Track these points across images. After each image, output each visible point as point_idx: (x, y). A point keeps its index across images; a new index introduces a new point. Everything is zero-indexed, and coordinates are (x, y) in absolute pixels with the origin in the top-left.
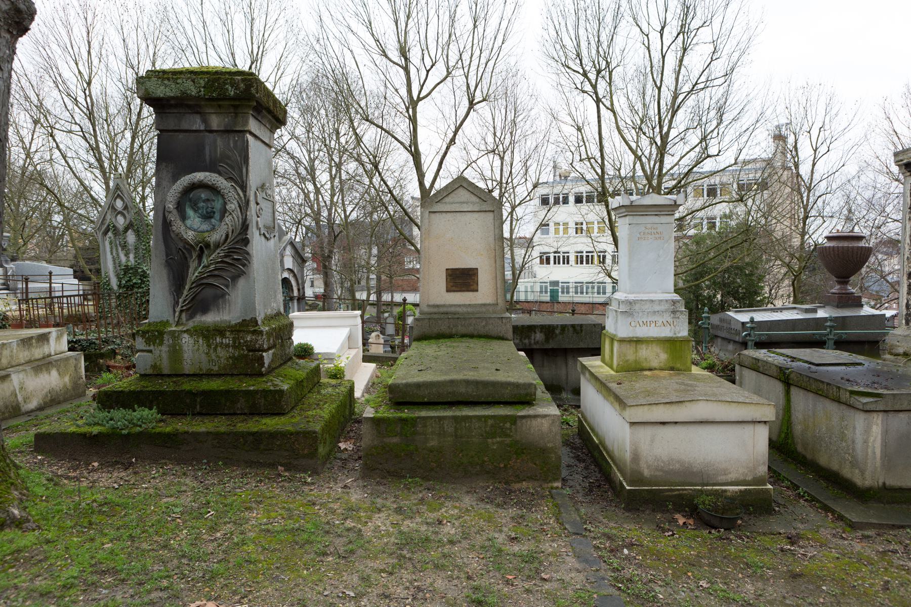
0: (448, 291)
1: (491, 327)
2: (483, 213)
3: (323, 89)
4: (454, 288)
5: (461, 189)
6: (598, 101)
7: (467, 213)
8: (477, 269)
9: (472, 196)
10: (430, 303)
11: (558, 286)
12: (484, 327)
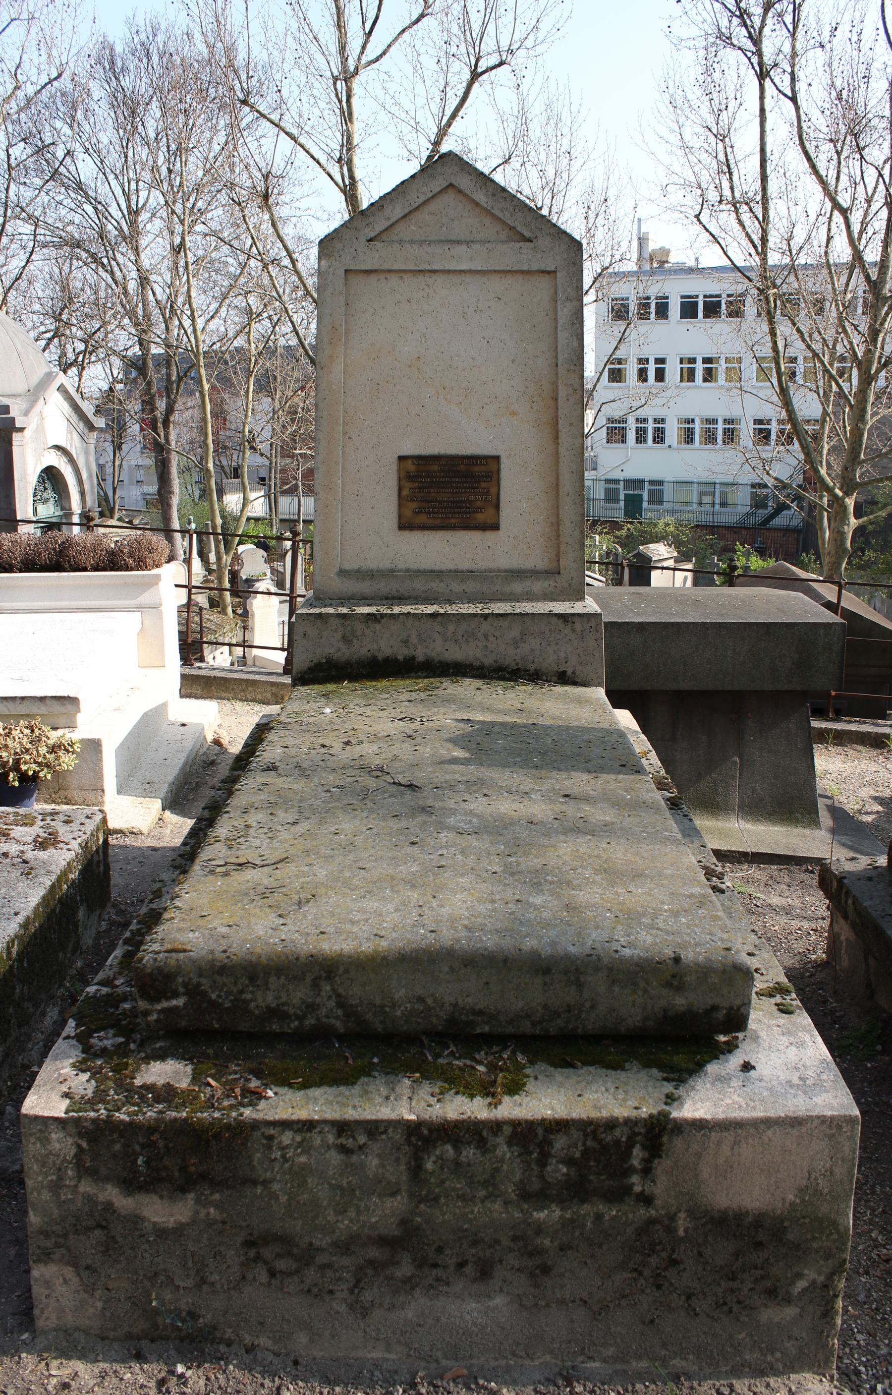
0: (404, 525)
1: (534, 643)
2: (520, 278)
4: (422, 519)
5: (450, 198)
6: (763, 75)
7: (468, 278)
8: (497, 458)
9: (487, 221)
10: (347, 566)
11: (643, 488)
12: (516, 643)
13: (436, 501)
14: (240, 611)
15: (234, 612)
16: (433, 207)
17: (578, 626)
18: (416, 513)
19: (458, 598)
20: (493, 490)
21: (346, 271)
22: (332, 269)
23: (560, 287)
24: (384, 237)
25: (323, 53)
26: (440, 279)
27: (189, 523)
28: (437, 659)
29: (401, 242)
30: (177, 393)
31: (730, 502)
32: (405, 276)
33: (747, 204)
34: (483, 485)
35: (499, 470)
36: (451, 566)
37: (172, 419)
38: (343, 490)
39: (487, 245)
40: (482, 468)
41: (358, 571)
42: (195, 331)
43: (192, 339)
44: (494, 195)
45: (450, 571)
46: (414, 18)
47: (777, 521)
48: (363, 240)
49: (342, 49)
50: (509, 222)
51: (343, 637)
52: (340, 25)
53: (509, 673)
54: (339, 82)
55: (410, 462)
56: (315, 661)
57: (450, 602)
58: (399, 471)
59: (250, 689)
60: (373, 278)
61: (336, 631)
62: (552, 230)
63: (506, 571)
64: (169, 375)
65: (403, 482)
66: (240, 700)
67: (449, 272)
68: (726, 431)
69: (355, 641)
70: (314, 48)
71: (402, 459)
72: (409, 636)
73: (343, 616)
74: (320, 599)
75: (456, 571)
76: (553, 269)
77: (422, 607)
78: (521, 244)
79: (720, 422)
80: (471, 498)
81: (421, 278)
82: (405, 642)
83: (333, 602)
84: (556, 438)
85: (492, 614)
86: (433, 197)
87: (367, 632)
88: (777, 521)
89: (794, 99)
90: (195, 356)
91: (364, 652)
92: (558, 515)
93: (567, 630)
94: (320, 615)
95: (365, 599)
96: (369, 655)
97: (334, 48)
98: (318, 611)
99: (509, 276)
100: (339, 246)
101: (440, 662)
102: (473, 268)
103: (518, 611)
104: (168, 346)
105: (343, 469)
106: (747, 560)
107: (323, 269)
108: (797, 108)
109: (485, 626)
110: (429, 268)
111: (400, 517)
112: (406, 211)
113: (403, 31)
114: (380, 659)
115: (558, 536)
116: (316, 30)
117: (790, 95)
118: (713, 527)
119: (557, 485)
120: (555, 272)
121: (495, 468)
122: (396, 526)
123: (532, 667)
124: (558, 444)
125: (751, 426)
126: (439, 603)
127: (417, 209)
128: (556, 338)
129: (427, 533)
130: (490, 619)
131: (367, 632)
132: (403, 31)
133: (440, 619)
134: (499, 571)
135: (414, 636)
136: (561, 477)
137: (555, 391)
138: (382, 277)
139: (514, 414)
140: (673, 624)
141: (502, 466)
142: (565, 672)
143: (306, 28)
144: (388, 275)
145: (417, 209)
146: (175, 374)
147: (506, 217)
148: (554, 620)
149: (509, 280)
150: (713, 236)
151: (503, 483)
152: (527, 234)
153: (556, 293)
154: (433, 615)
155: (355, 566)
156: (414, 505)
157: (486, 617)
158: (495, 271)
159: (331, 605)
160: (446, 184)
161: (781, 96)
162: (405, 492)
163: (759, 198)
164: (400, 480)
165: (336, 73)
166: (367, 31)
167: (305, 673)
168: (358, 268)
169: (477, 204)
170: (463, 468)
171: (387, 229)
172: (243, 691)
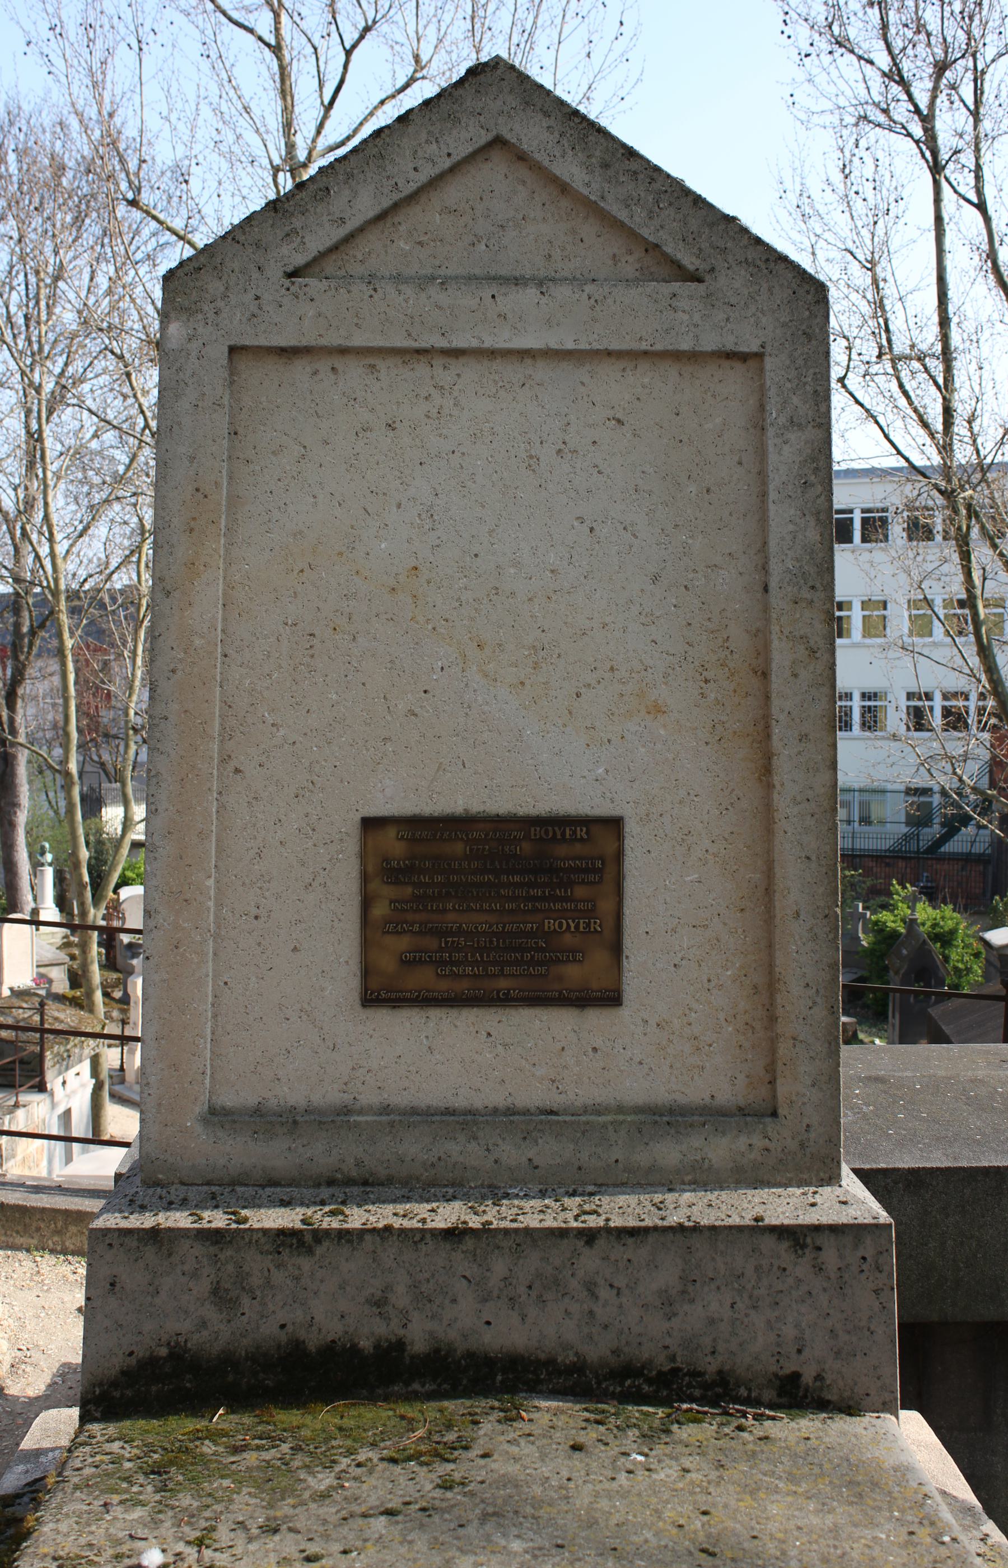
2: (671, 370)
3: (222, 553)
4: (424, 978)
7: (541, 371)
8: (615, 824)
9: (589, 229)
10: (228, 1099)
13: (460, 932)
14: (118, 994)
15: (106, 995)
16: (453, 193)
17: (830, 1257)
18: (408, 962)
19: (515, 1182)
20: (606, 906)
21: (232, 350)
22: (195, 345)
23: (772, 392)
24: (329, 266)
25: (257, 131)
26: (470, 372)
27: (43, 853)
28: (461, 1347)
29: (371, 279)
30: (29, 653)
31: (874, 817)
32: (381, 364)
33: (919, 359)
34: (580, 892)
35: (619, 856)
36: (497, 1098)
37: (20, 691)
38: (219, 905)
39: (589, 288)
40: (578, 848)
41: (258, 1112)
42: (52, 554)
43: (47, 563)
44: (606, 166)
45: (495, 1111)
46: (399, 84)
47: (955, 846)
48: (275, 272)
49: (288, 126)
50: (645, 232)
51: (216, 1291)
52: (285, 92)
53: (649, 1381)
54: (281, 175)
55: (392, 832)
56: (141, 1353)
57: (497, 1194)
58: (363, 856)
59: (73, 1229)
60: (300, 369)
61: (195, 1275)
62: (752, 254)
63: (638, 1110)
64: (17, 626)
65: (374, 885)
66: (52, 1251)
67: (493, 353)
68: (866, 711)
69: (246, 1301)
70: (243, 123)
71: (370, 824)
72: (388, 1288)
73: (215, 1236)
74: (157, 1184)
75: (511, 1111)
76: (754, 348)
77: (422, 1209)
78: (676, 286)
79: (857, 696)
80: (550, 924)
81: (421, 369)
82: (379, 1303)
83: (192, 1193)
84: (766, 770)
85: (607, 1230)
86: (453, 170)
87: (278, 1277)
88: (955, 846)
89: (981, 207)
90: (53, 595)
91: (269, 1329)
92: (771, 966)
93: (802, 1268)
94: (155, 1233)
95: (274, 1183)
96: (283, 1337)
97: (274, 123)
98: (147, 1221)
99: (644, 366)
100: (215, 287)
101: (470, 1355)
102: (554, 345)
103: (674, 1219)
104: (17, 580)
105: (220, 850)
106: (913, 909)
107: (173, 344)
108: (987, 220)
109: (590, 1261)
110: (442, 343)
111: (367, 971)
112: (386, 203)
113: (382, 102)
114: (312, 1346)
115: (772, 1019)
116: (247, 94)
117: (975, 200)
118: (854, 856)
119: (769, 891)
120: (759, 356)
121: (610, 848)
122: (355, 997)
123: (711, 1366)
124: (770, 786)
125: (903, 703)
126: (466, 1197)
127: (412, 198)
128: (763, 520)
129: (435, 1013)
130: (601, 1243)
131: (278, 1277)
132: (382, 102)
133: (469, 1243)
134: (620, 1109)
135: (401, 1289)
136: (778, 871)
137: (763, 652)
138: (323, 365)
139: (657, 710)
140: (986, 1171)
141: (629, 843)
142: (796, 1376)
143: (232, 92)
144: (339, 362)
145: (412, 198)
146: (27, 623)
147: (637, 219)
148: (768, 1243)
149: (644, 375)
150: (867, 411)
151: (630, 886)
152: (689, 261)
153: (762, 407)
154: (454, 1235)
155: (248, 1098)
156: (403, 943)
157: (589, 1236)
158: (609, 353)
159: (183, 1204)
160: (485, 138)
161: (962, 202)
162: (380, 910)
163: (938, 348)
164: (365, 878)
165: (277, 161)
166: (326, 102)
167: (114, 1384)
168: (262, 342)
169: (564, 188)
170: (527, 847)
171: (335, 248)
172: (58, 1232)
